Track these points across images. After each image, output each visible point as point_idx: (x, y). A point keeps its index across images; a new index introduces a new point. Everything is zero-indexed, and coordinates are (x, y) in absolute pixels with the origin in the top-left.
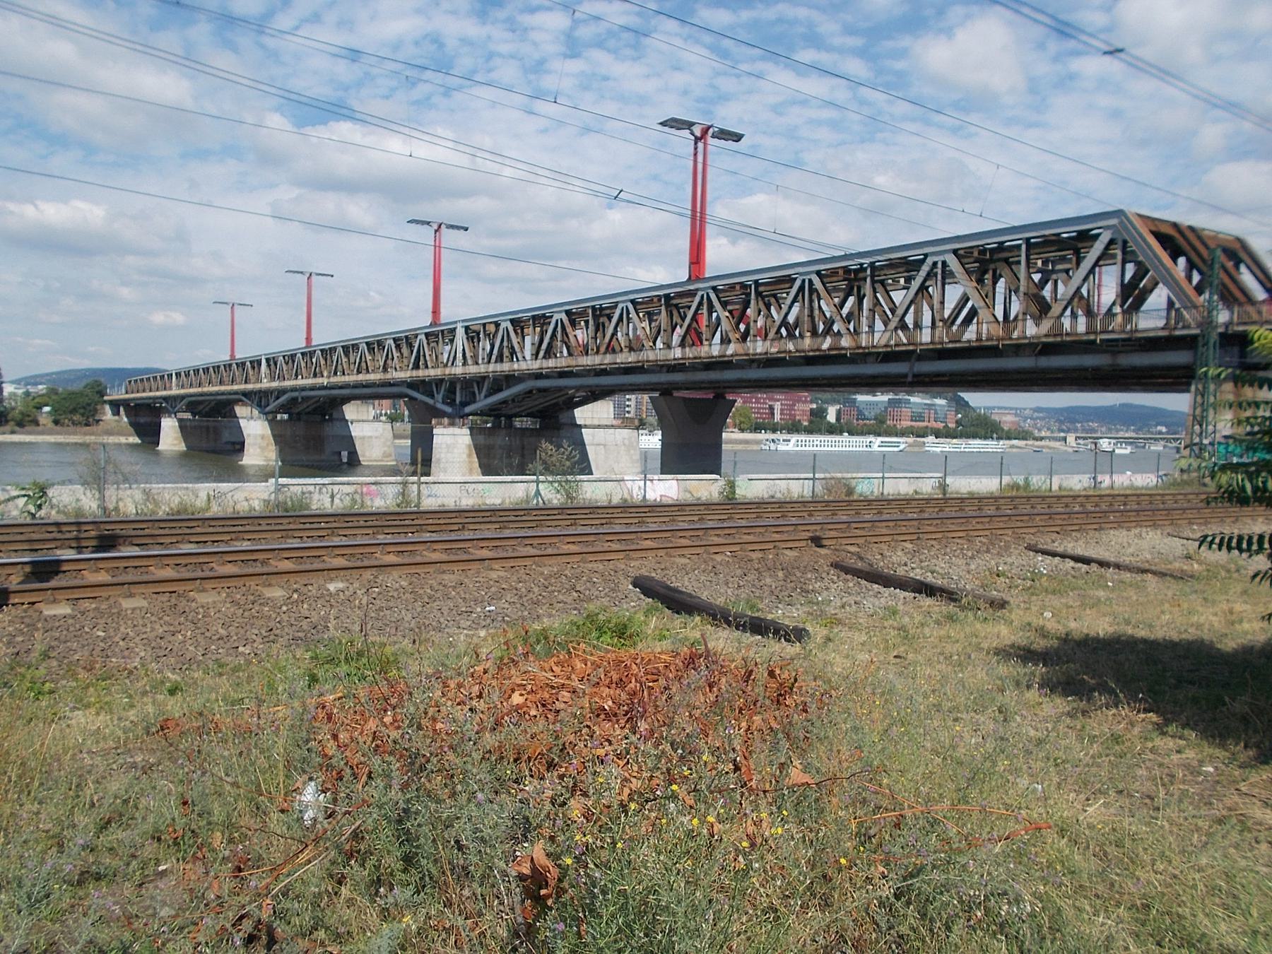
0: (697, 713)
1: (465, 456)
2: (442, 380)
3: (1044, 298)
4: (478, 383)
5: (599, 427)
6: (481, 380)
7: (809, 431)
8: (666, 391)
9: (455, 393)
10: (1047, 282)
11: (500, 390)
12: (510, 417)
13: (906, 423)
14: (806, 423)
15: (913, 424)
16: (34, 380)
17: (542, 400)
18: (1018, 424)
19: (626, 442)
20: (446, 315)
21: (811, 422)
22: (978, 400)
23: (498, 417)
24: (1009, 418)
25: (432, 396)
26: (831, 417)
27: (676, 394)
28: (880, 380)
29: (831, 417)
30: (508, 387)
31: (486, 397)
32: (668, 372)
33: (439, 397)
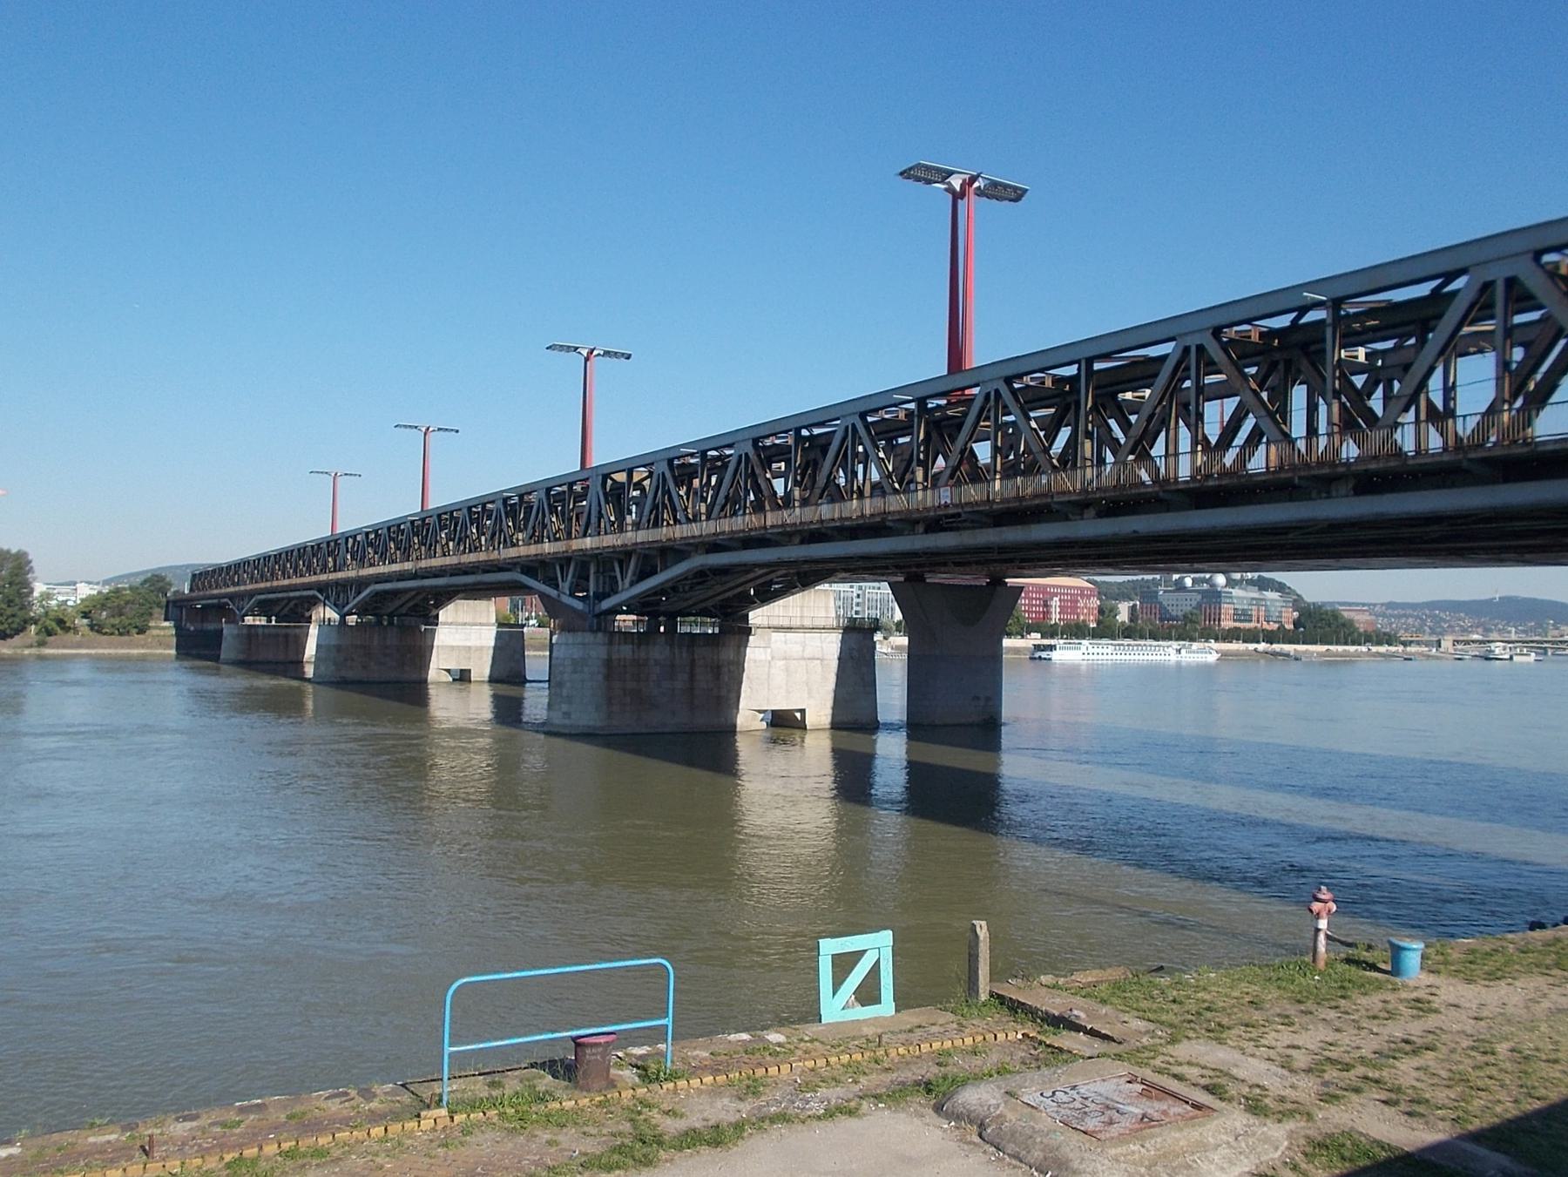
0: (1347, 1154)
1: (600, 677)
2: (568, 560)
3: (1371, 410)
4: (621, 563)
5: (789, 629)
6: (623, 555)
7: (1097, 634)
8: (915, 579)
9: (587, 579)
10: (1377, 385)
11: (653, 572)
12: (672, 617)
13: (1227, 624)
14: (1093, 625)
15: (1238, 624)
16: (106, 582)
17: (719, 589)
18: (1372, 623)
19: (855, 654)
20: (979, 354)
21: (1099, 623)
22: (1320, 585)
23: (654, 615)
24: (1365, 617)
25: (556, 587)
26: (1123, 616)
27: (931, 579)
28: (1076, 551)
29: (1123, 616)
30: (665, 567)
31: (632, 584)
32: (802, 542)
33: (565, 586)
